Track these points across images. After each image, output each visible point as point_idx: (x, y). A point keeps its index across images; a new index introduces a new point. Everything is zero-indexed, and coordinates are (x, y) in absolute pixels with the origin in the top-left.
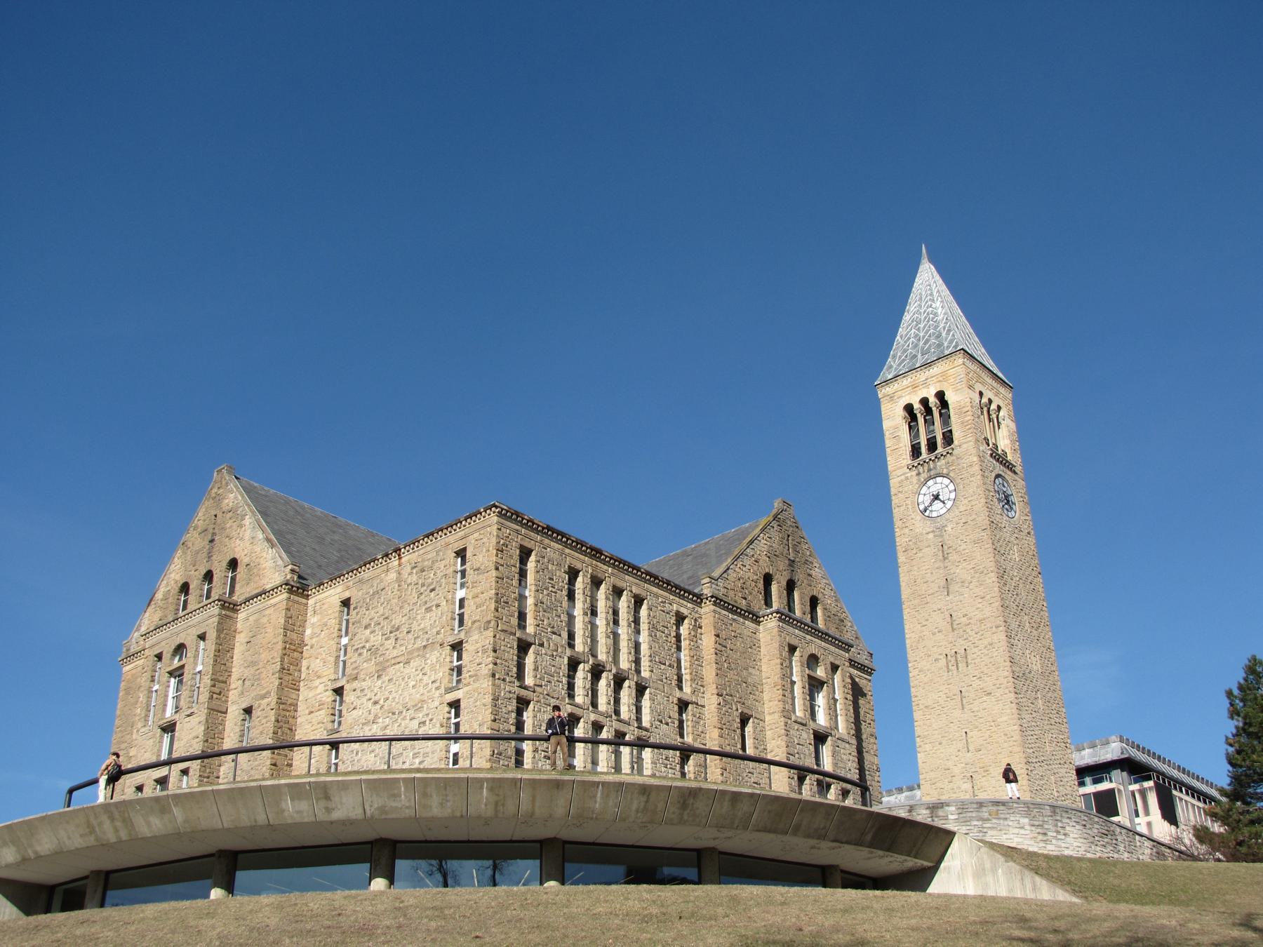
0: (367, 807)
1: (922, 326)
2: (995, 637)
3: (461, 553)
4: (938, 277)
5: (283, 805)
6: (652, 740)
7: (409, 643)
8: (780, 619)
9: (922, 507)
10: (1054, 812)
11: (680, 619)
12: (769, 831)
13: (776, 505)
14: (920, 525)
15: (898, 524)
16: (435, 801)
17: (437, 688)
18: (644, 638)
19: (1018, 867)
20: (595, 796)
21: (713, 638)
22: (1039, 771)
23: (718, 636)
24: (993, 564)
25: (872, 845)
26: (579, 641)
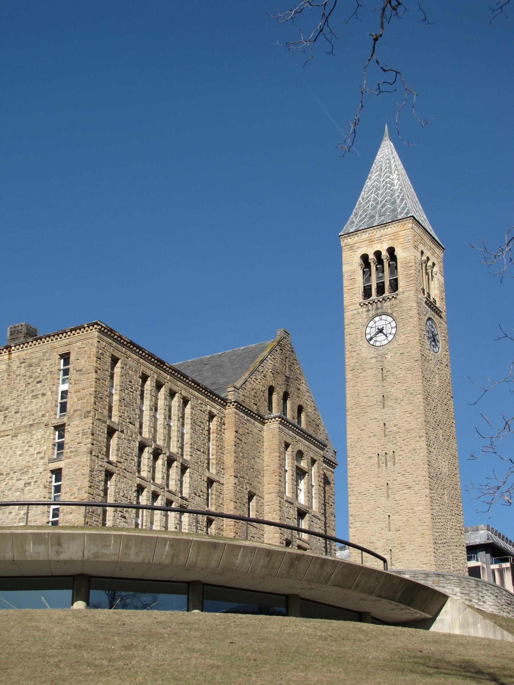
0: (86, 553)
3: (66, 357)
5: (27, 547)
6: (189, 508)
8: (281, 423)
9: (368, 337)
10: (477, 585)
11: (212, 416)
12: (341, 587)
13: (279, 332)
15: (348, 348)
16: (133, 551)
17: (42, 458)
18: (187, 429)
19: (492, 624)
20: (237, 555)
21: (234, 433)
22: (442, 550)
23: (237, 432)
25: (400, 601)
26: (145, 430)
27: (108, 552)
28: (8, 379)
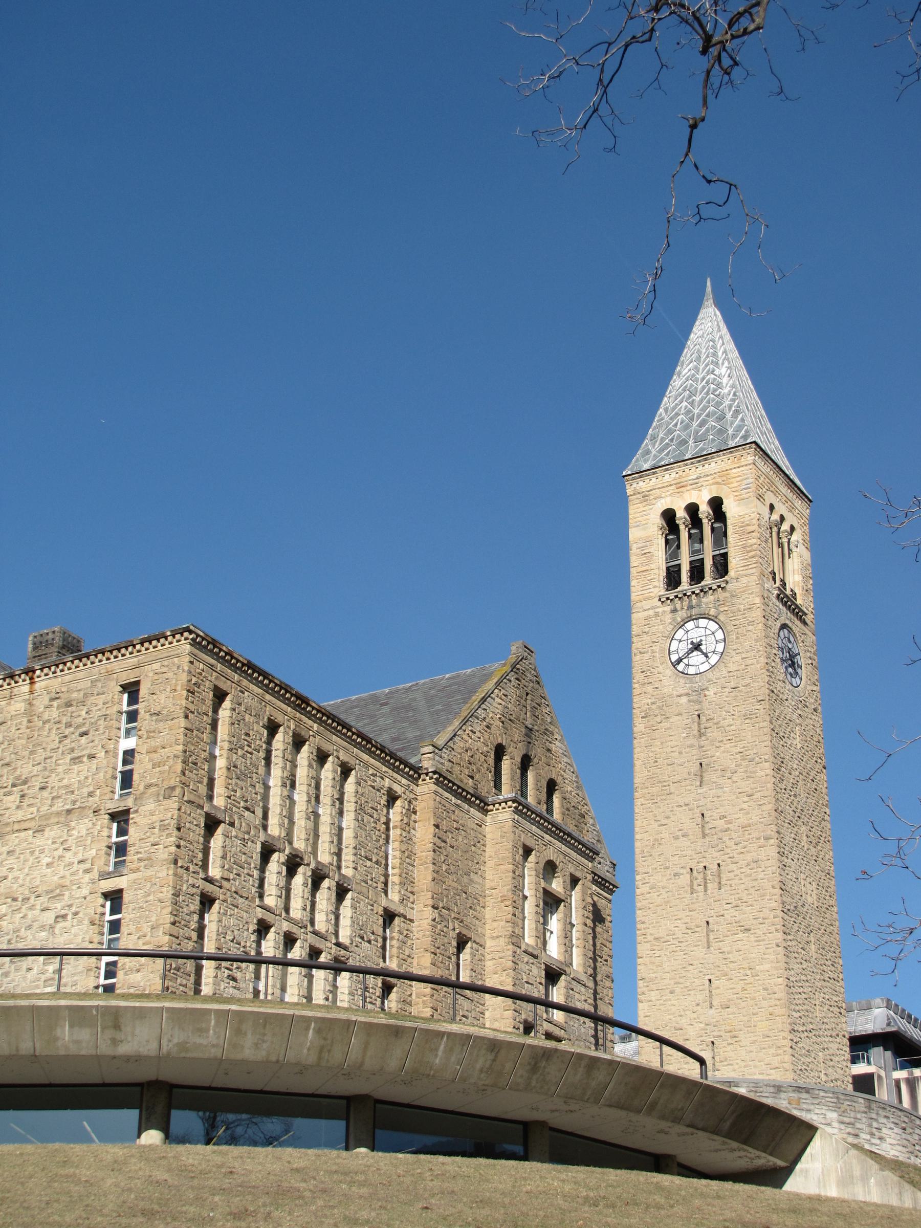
0: (164, 1042)
1: (697, 399)
2: (763, 853)
3: (132, 690)
4: (724, 330)
5: (59, 1032)
6: (351, 962)
7: (43, 804)
9: (674, 658)
10: (869, 1108)
11: (392, 798)
12: (622, 1108)
13: (514, 649)
14: (669, 682)
15: (638, 677)
16: (249, 1039)
17: (87, 871)
18: (348, 821)
20: (437, 1050)
23: (437, 826)
24: (768, 750)
25: (730, 1135)
27: (204, 1042)
28: (28, 728)
